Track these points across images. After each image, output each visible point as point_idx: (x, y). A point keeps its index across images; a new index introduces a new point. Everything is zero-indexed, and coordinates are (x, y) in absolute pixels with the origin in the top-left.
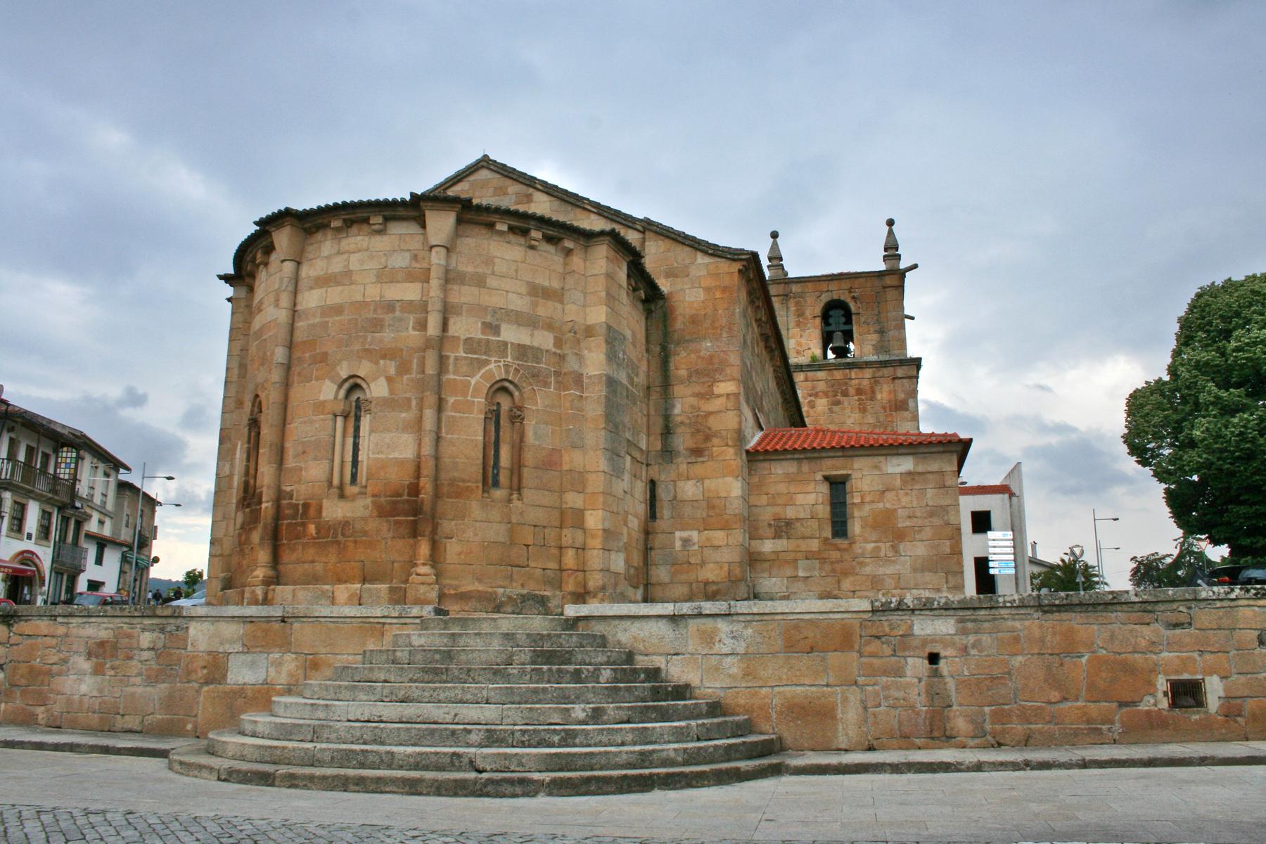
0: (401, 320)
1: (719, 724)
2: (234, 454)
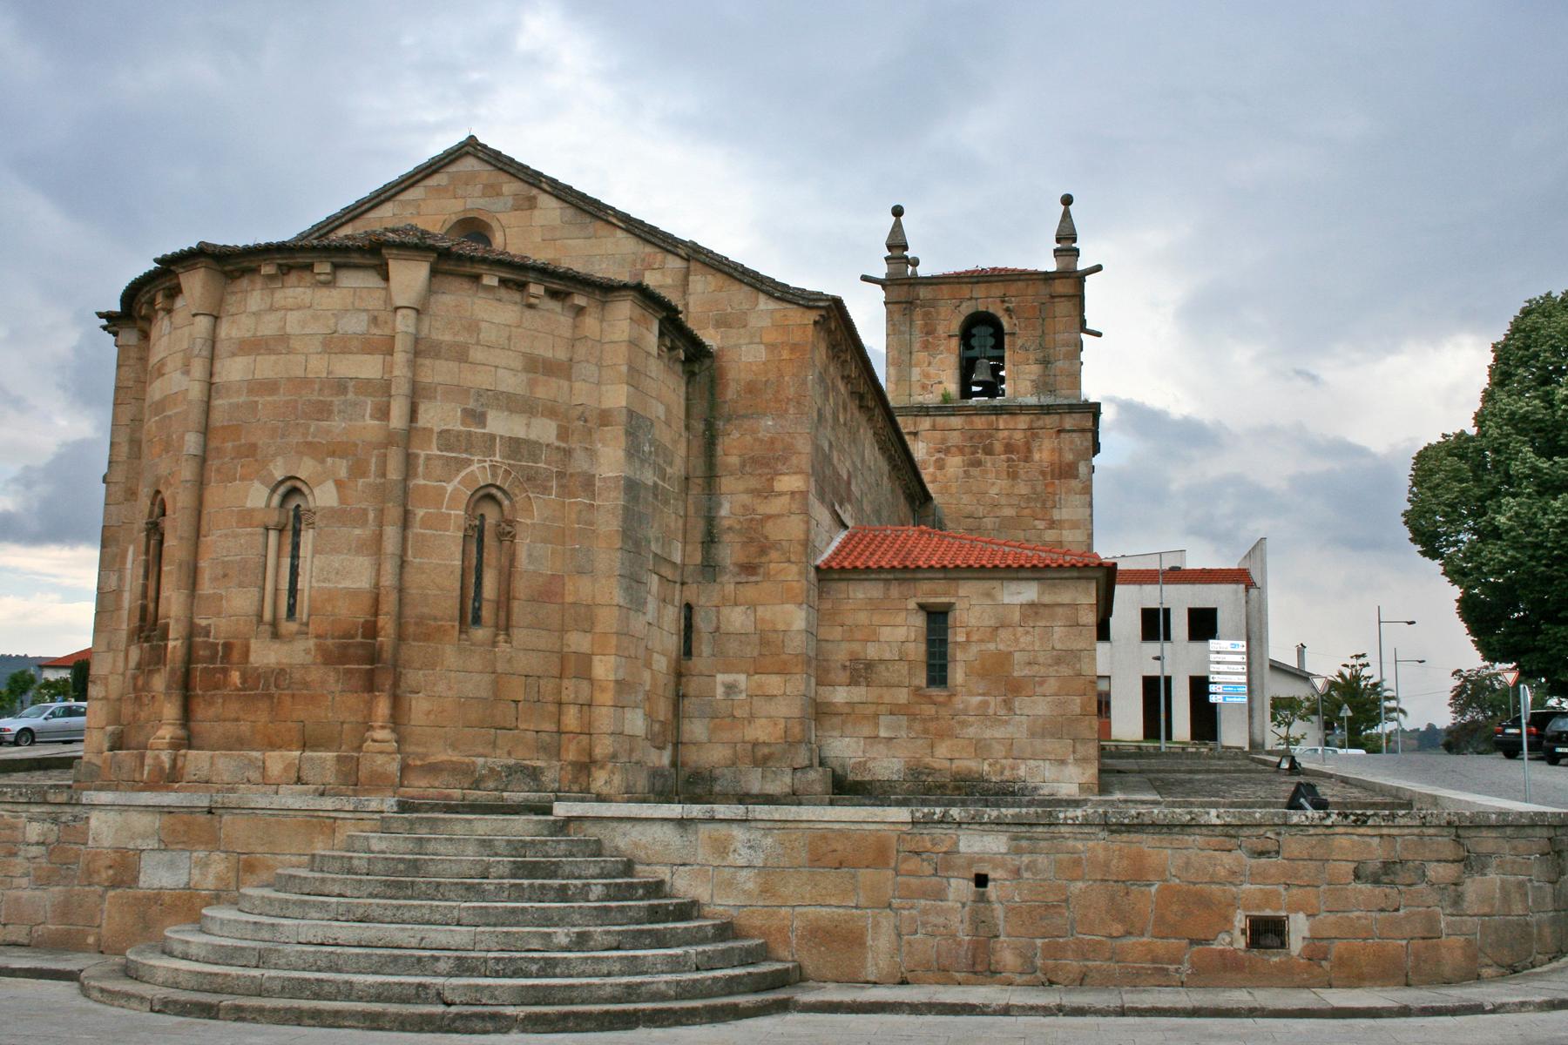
0: (355, 404)
1: (723, 952)
2: (123, 561)
